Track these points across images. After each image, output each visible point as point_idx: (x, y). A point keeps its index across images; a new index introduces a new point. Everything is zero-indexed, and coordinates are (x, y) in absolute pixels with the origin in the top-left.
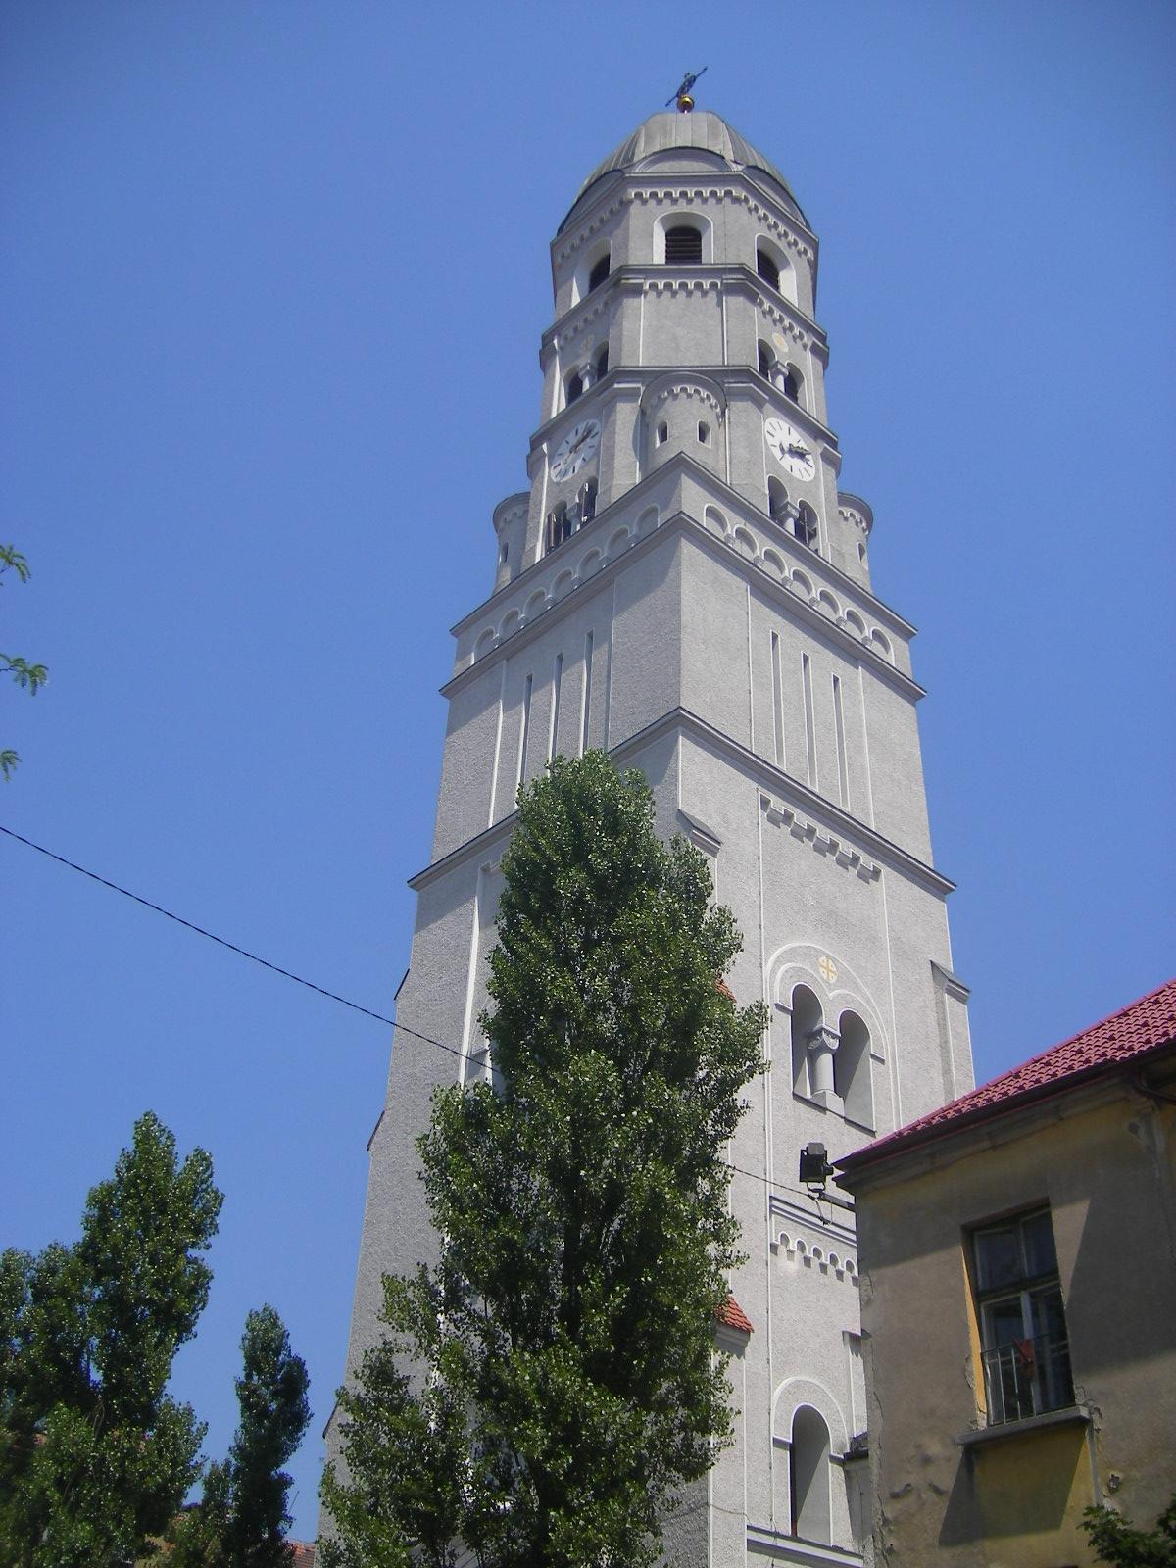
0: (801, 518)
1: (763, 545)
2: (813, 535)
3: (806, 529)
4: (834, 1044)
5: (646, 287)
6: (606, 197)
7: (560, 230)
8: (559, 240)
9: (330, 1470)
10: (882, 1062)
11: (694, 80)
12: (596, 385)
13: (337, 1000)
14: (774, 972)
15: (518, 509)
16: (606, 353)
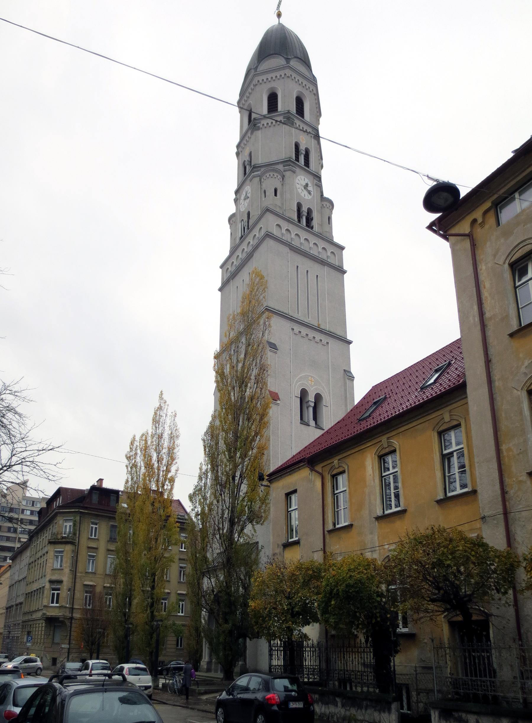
4: (313, 405)
6: (264, 72)
8: (245, 179)
9: (245, 161)
14: (295, 386)
15: (233, 219)
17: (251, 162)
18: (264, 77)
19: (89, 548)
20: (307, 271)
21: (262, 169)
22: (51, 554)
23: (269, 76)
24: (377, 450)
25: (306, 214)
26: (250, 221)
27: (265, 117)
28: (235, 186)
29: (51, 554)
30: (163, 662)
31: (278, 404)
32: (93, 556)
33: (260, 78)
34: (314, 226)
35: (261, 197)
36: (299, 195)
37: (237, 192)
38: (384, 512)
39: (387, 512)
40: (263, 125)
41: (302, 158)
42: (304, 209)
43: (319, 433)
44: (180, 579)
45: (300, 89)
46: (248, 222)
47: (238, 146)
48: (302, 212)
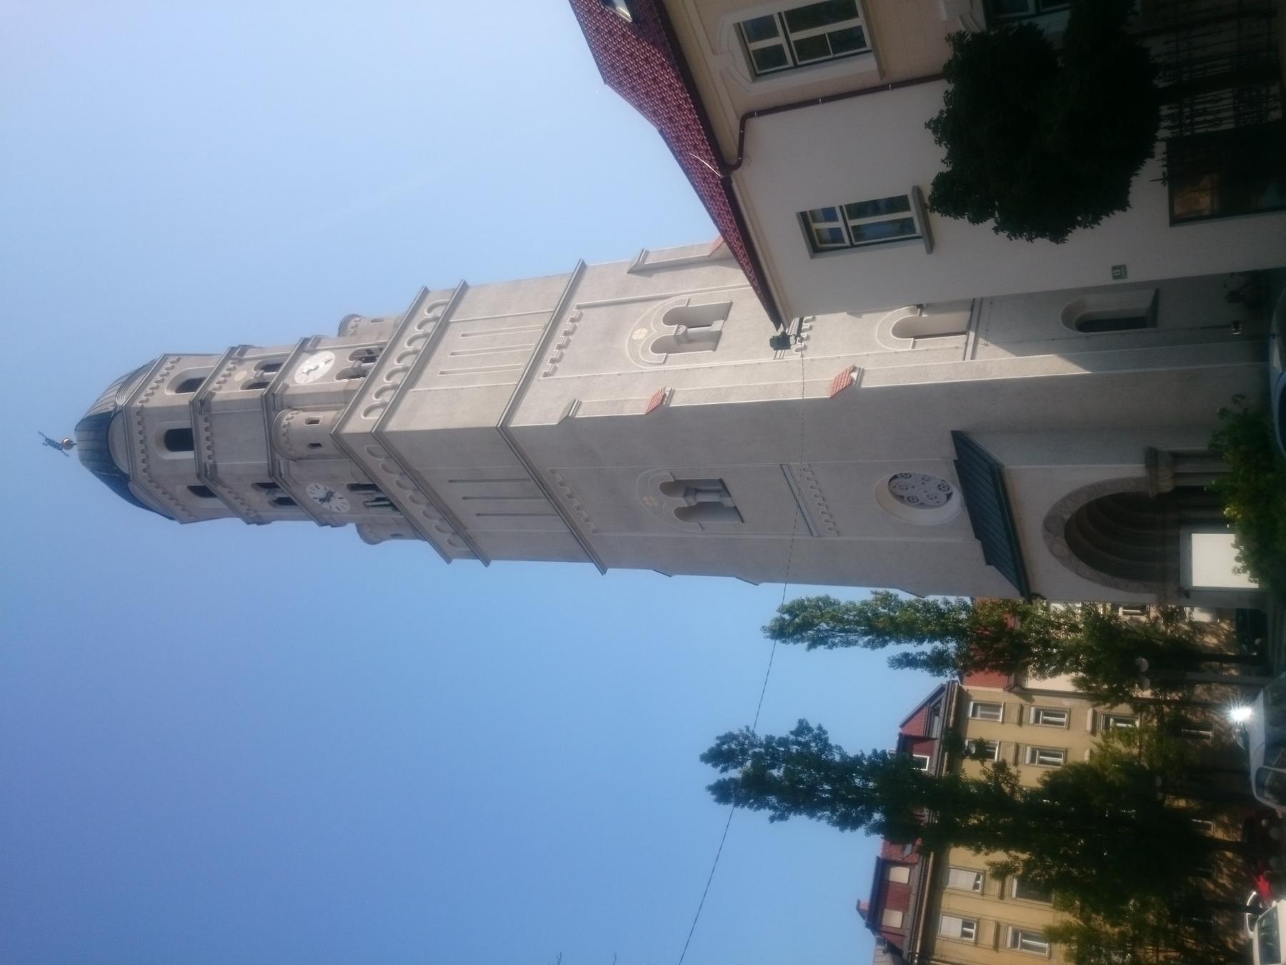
0: (360, 359)
1: (383, 381)
2: (369, 351)
3: (369, 356)
4: (683, 328)
5: (211, 461)
7: (172, 518)
10: (689, 300)
11: (49, 439)
12: (283, 488)
13: (693, 932)
16: (258, 484)
19: (996, 947)
21: (278, 456)
24: (947, 695)
30: (1256, 583)
32: (1015, 934)
39: (918, 231)
44: (1061, 724)
45: (164, 386)
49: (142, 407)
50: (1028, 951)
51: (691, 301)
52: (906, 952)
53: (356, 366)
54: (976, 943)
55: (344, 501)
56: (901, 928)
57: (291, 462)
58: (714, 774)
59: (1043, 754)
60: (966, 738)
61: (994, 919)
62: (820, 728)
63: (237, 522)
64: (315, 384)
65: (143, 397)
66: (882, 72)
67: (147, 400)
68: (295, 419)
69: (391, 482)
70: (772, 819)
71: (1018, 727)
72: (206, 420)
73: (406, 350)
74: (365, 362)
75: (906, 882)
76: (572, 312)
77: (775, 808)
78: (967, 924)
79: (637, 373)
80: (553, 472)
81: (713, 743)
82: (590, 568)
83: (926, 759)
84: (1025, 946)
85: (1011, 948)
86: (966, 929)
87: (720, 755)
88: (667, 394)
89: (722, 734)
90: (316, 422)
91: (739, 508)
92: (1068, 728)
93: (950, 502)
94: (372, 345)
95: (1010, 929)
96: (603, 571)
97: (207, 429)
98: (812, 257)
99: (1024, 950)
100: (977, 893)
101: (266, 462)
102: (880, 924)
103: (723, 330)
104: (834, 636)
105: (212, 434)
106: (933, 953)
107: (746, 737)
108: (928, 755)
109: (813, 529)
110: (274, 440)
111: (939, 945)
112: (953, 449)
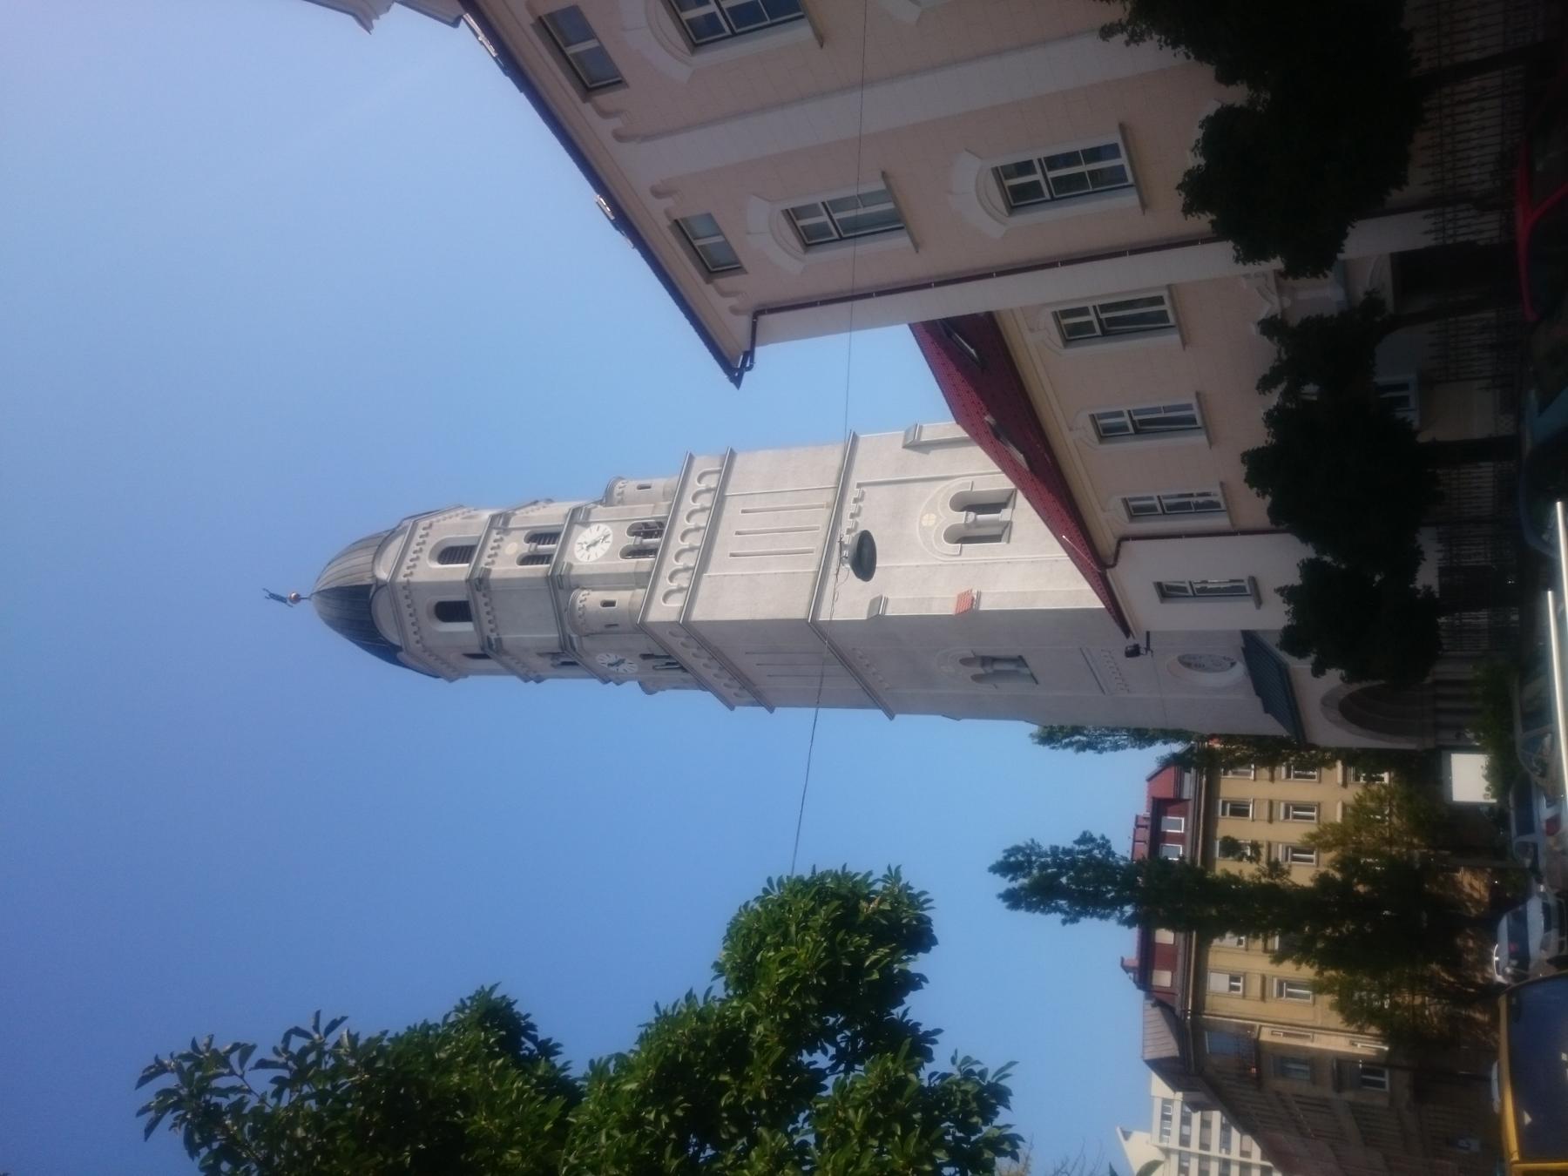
1: (671, 564)
7: (437, 677)
9: (553, 665)
17: (553, 654)
18: (410, 630)
19: (1263, 998)
20: (738, 533)
22: (1280, 1084)
23: (408, 621)
25: (639, 539)
26: (657, 653)
27: (479, 629)
28: (595, 683)
29: (1280, 1084)
31: (979, 594)
32: (1280, 984)
33: (413, 638)
34: (659, 520)
35: (617, 633)
36: (607, 555)
37: (605, 681)
38: (1131, 186)
40: (492, 631)
41: (544, 548)
42: (632, 541)
43: (1021, 500)
45: (425, 555)
46: (658, 657)
47: (526, 679)
48: (637, 546)
49: (408, 582)
50: (1292, 999)
51: (975, 484)
52: (1178, 1010)
53: (638, 542)
54: (1244, 996)
55: (634, 665)
56: (1172, 985)
57: (583, 638)
58: (1004, 884)
59: (1296, 809)
60: (1218, 798)
61: (1260, 972)
62: (1103, 837)
63: (514, 680)
64: (599, 563)
65: (404, 570)
66: (1233, 525)
67: (411, 574)
68: (589, 599)
69: (687, 655)
70: (1064, 922)
71: (1271, 783)
72: (484, 596)
73: (688, 528)
74: (645, 538)
75: (1172, 943)
76: (853, 492)
77: (1066, 913)
78: (1234, 978)
79: (935, 565)
80: (854, 649)
81: (1000, 857)
82: (878, 715)
83: (1181, 821)
84: (1290, 995)
85: (1277, 997)
86: (1233, 983)
87: (1005, 868)
88: (975, 597)
89: (1008, 846)
90: (612, 604)
91: (1035, 675)
92: (1320, 781)
93: (1233, 669)
94: (648, 519)
95: (1275, 980)
96: (891, 716)
97: (486, 604)
98: (1162, 602)
99: (1289, 999)
100: (1241, 949)
101: (557, 635)
102: (1152, 986)
103: (1014, 520)
104: (1103, 742)
105: (493, 608)
106: (1204, 1009)
107: (1032, 849)
108: (1180, 815)
109: (1104, 687)
110: (563, 613)
111: (1208, 999)
112: (1242, 640)
